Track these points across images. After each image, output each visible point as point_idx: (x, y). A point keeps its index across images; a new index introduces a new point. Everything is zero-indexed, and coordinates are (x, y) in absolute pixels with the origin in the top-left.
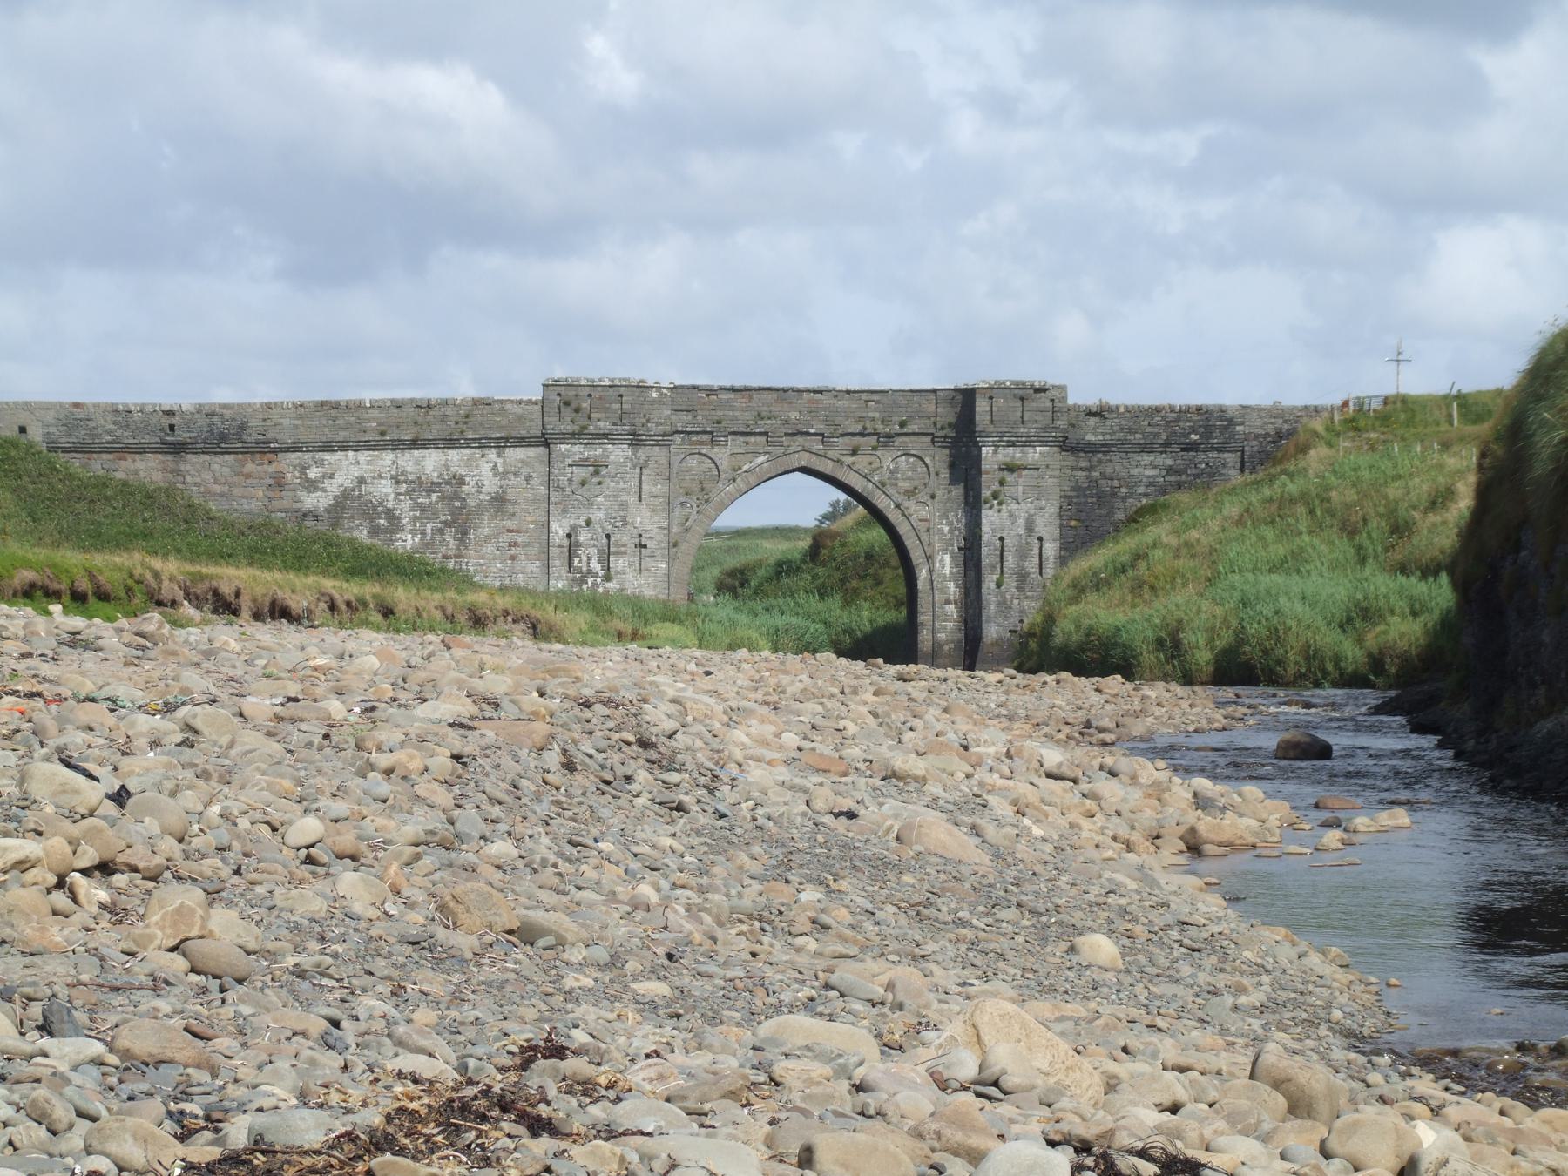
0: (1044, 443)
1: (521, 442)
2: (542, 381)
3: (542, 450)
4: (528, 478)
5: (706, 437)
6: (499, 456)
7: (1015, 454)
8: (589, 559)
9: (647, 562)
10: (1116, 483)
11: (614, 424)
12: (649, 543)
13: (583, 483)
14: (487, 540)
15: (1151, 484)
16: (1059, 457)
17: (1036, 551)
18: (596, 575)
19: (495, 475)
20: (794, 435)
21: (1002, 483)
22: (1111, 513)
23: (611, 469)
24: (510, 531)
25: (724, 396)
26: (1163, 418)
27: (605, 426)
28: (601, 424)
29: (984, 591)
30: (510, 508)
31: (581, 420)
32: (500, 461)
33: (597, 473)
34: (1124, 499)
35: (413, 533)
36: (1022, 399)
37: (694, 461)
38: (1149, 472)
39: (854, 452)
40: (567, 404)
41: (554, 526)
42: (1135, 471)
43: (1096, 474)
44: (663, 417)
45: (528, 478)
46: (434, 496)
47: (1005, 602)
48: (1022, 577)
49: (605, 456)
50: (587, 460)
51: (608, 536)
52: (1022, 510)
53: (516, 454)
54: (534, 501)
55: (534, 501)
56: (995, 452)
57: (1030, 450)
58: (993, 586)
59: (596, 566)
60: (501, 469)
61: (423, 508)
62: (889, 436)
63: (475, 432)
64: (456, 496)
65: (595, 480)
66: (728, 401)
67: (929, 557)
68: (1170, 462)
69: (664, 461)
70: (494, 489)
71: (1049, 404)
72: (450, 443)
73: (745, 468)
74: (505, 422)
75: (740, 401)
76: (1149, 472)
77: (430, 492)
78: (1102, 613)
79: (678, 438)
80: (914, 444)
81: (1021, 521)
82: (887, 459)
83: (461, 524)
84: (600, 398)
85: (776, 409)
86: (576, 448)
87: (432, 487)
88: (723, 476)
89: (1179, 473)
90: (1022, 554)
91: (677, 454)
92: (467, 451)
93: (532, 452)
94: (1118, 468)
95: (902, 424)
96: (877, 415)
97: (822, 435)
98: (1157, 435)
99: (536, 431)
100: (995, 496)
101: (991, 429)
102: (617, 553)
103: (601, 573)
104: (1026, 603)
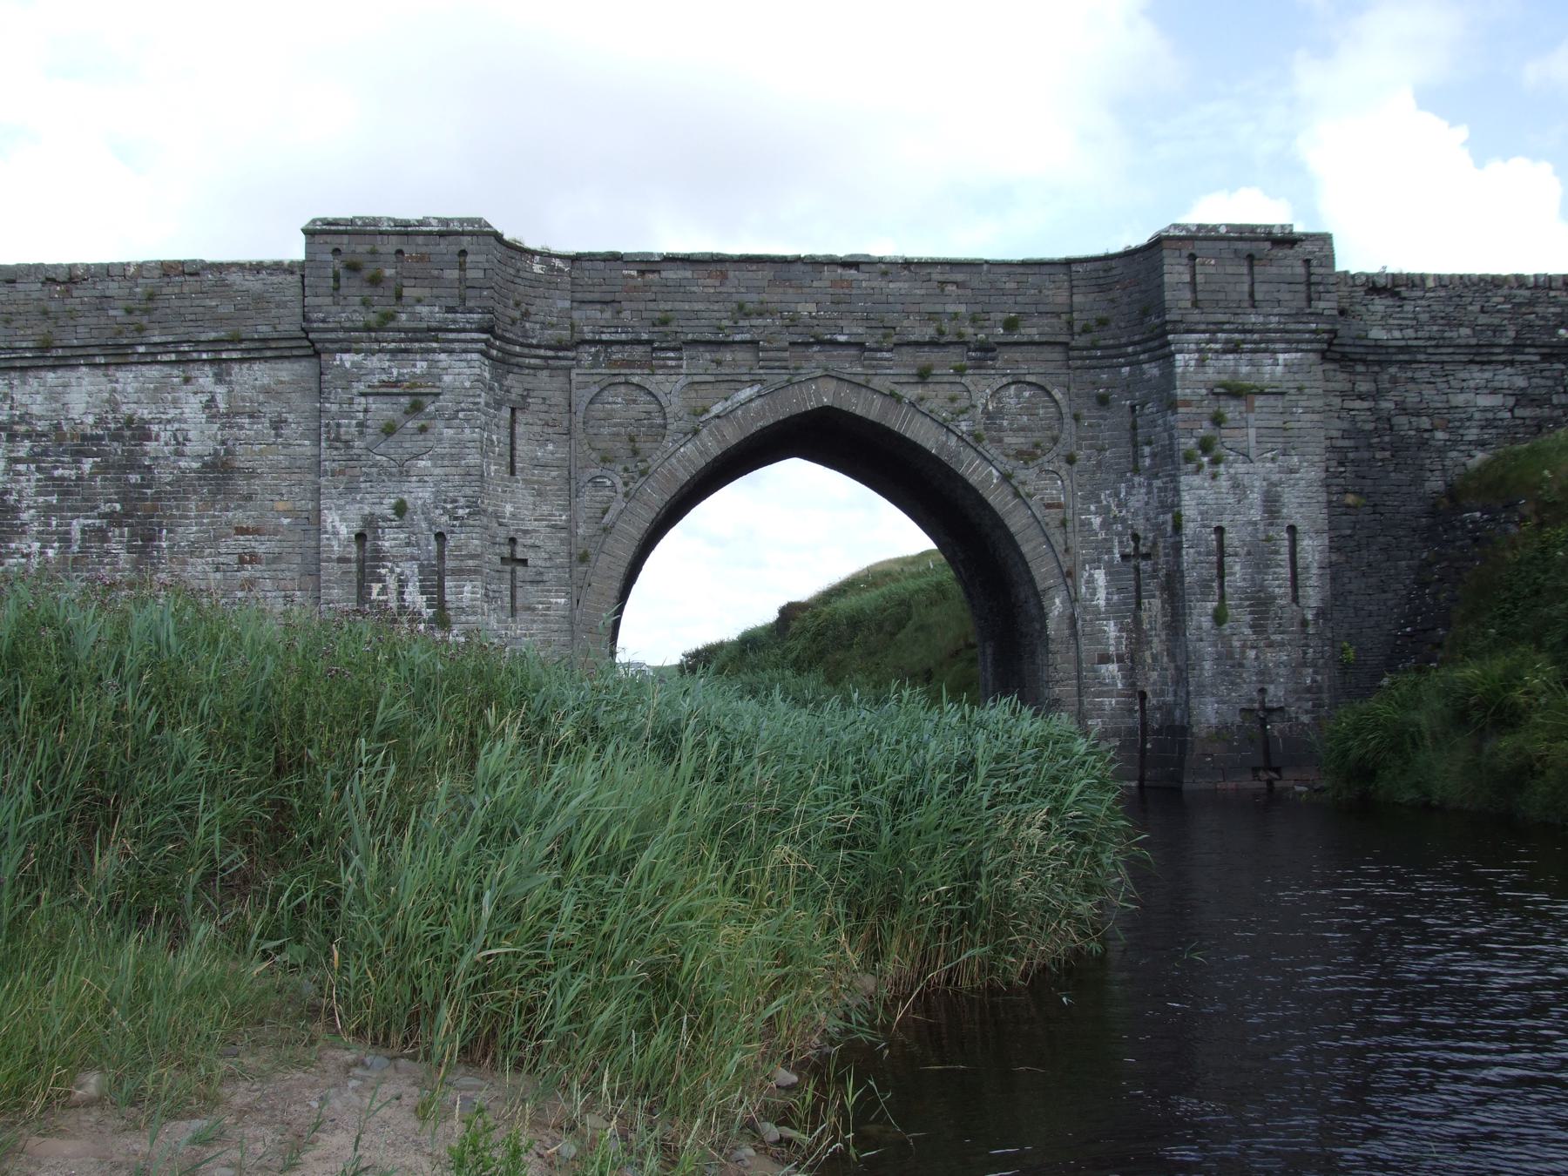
0: (1292, 345)
1: (262, 350)
2: (305, 222)
3: (302, 368)
4: (278, 424)
5: (639, 351)
6: (219, 379)
7: (1241, 367)
8: (402, 584)
9: (528, 594)
10: (1425, 423)
11: (450, 310)
12: (531, 556)
13: (389, 430)
14: (195, 549)
15: (1488, 424)
16: (1318, 370)
17: (1284, 556)
18: (415, 617)
19: (212, 418)
20: (807, 344)
21: (1218, 420)
22: (1418, 481)
23: (446, 401)
24: (241, 531)
25: (671, 274)
26: (1508, 299)
27: (431, 314)
28: (423, 310)
29: (1191, 633)
30: (242, 485)
31: (383, 303)
32: (221, 391)
33: (416, 408)
34: (1442, 451)
35: (44, 539)
36: (1251, 258)
37: (616, 399)
38: (1484, 401)
39: (923, 376)
40: (353, 268)
41: (331, 518)
42: (1459, 399)
43: (1387, 405)
44: (553, 312)
45: (278, 424)
46: (87, 465)
47: (1230, 655)
48: (1261, 604)
49: (433, 375)
50: (395, 384)
51: (440, 537)
52: (1257, 474)
53: (254, 377)
54: (289, 470)
55: (289, 470)
56: (1201, 363)
57: (1266, 359)
58: (1207, 623)
59: (415, 598)
60: (222, 407)
61: (63, 488)
62: (986, 349)
63: (165, 330)
64: (132, 463)
65: (412, 425)
66: (680, 284)
67: (1069, 575)
68: (1521, 382)
69: (558, 398)
70: (207, 448)
71: (1300, 270)
72: (117, 355)
73: (717, 409)
74: (226, 309)
75: (706, 284)
76: (1484, 401)
77: (79, 454)
78: (359, 789)
79: (586, 354)
80: (1034, 366)
81: (1255, 497)
82: (981, 390)
83: (143, 518)
84: (421, 258)
85: (773, 297)
86: (374, 362)
87: (84, 445)
88: (673, 426)
89: (1534, 402)
90: (1260, 558)
91: (586, 385)
92: (154, 372)
93: (286, 371)
94: (1428, 392)
95: (1010, 325)
96: (962, 309)
97: (861, 346)
98: (1497, 330)
99: (290, 324)
100: (1206, 446)
101: (1195, 316)
102: (458, 572)
103: (428, 613)
104: (1270, 656)
